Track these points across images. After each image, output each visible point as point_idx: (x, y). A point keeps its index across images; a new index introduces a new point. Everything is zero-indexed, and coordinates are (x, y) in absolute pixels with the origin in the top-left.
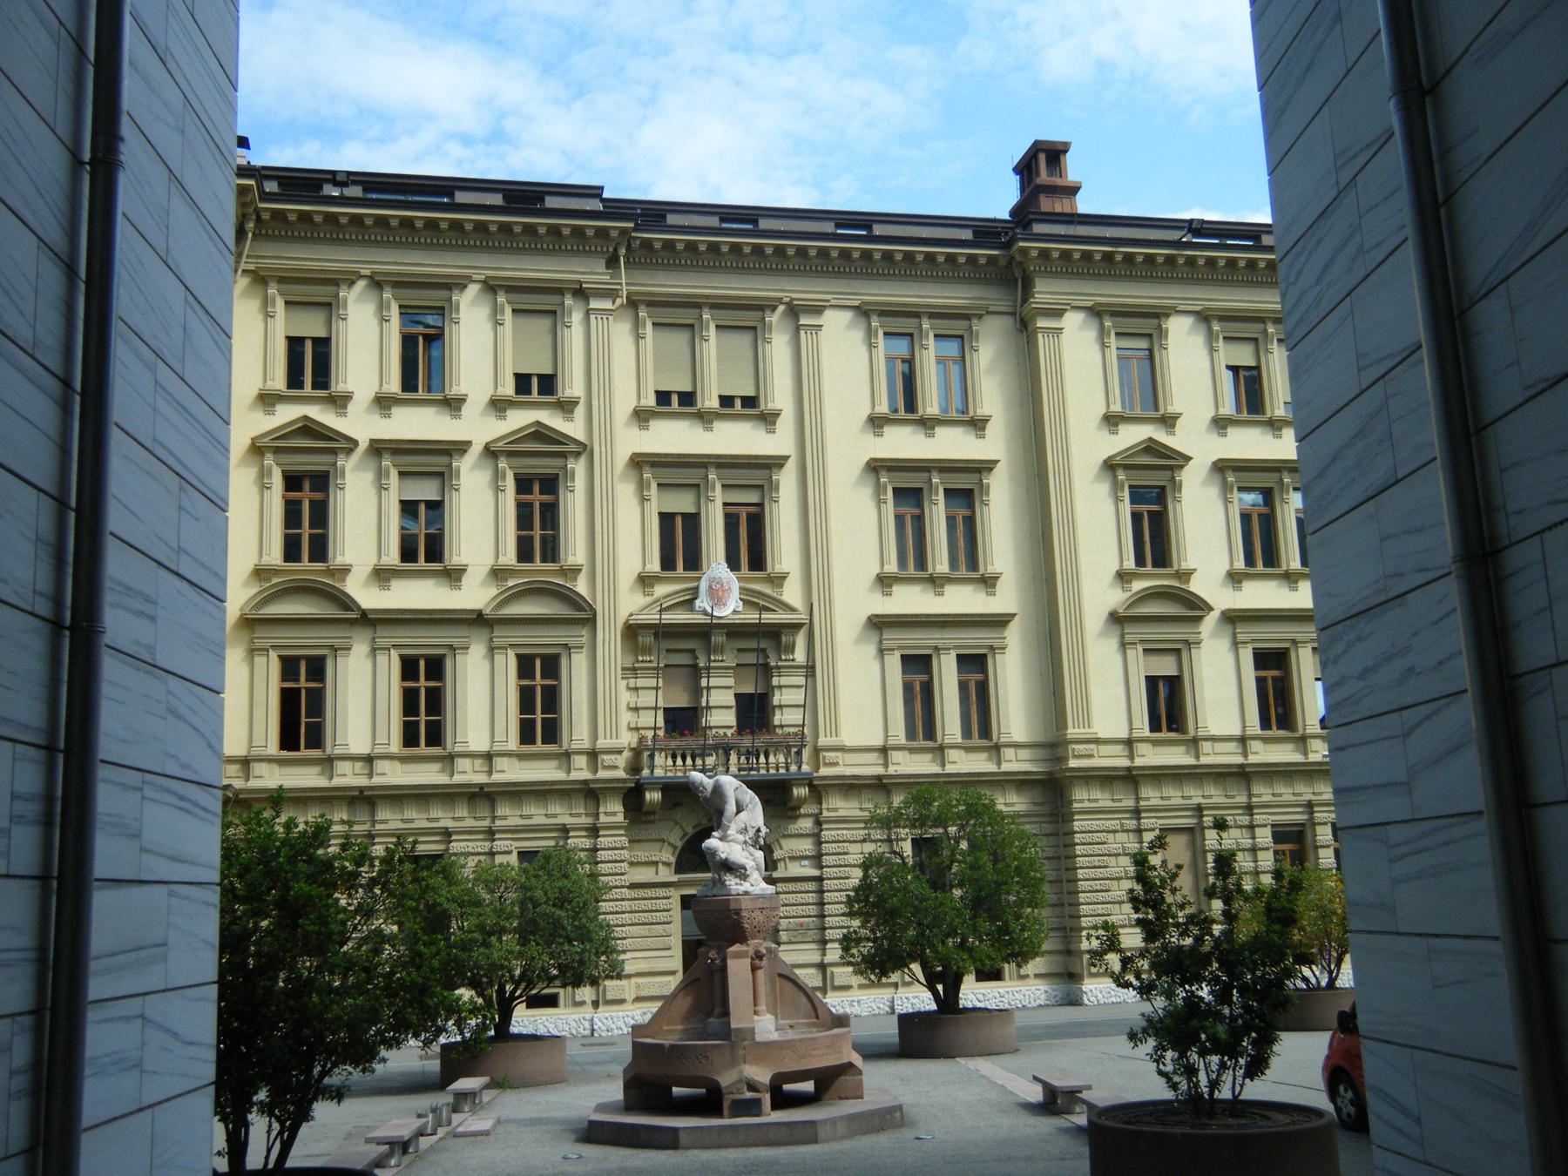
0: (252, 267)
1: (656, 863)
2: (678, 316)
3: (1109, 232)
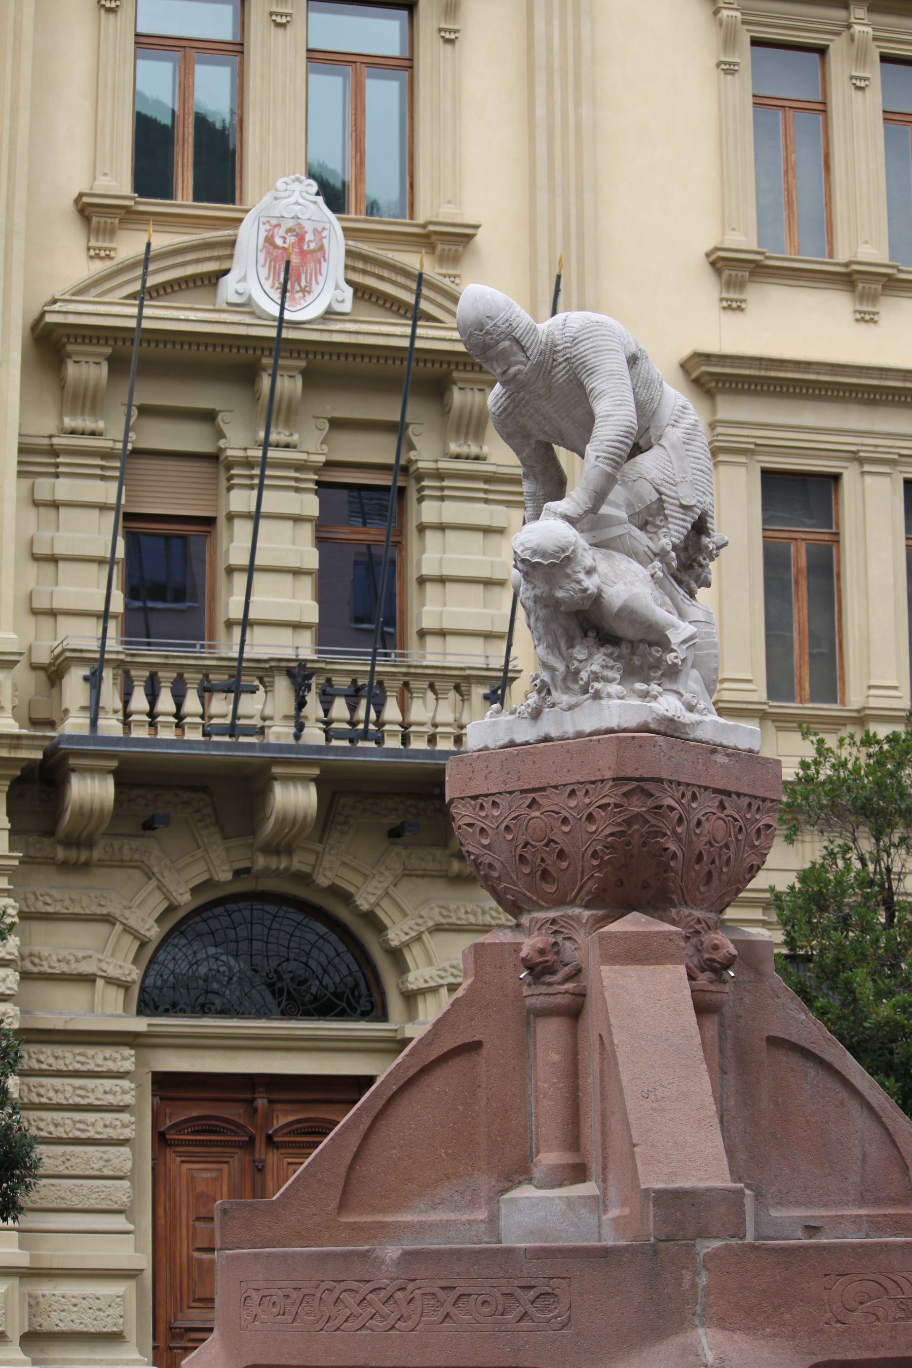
1: (89, 979)
3: (197, 1159)
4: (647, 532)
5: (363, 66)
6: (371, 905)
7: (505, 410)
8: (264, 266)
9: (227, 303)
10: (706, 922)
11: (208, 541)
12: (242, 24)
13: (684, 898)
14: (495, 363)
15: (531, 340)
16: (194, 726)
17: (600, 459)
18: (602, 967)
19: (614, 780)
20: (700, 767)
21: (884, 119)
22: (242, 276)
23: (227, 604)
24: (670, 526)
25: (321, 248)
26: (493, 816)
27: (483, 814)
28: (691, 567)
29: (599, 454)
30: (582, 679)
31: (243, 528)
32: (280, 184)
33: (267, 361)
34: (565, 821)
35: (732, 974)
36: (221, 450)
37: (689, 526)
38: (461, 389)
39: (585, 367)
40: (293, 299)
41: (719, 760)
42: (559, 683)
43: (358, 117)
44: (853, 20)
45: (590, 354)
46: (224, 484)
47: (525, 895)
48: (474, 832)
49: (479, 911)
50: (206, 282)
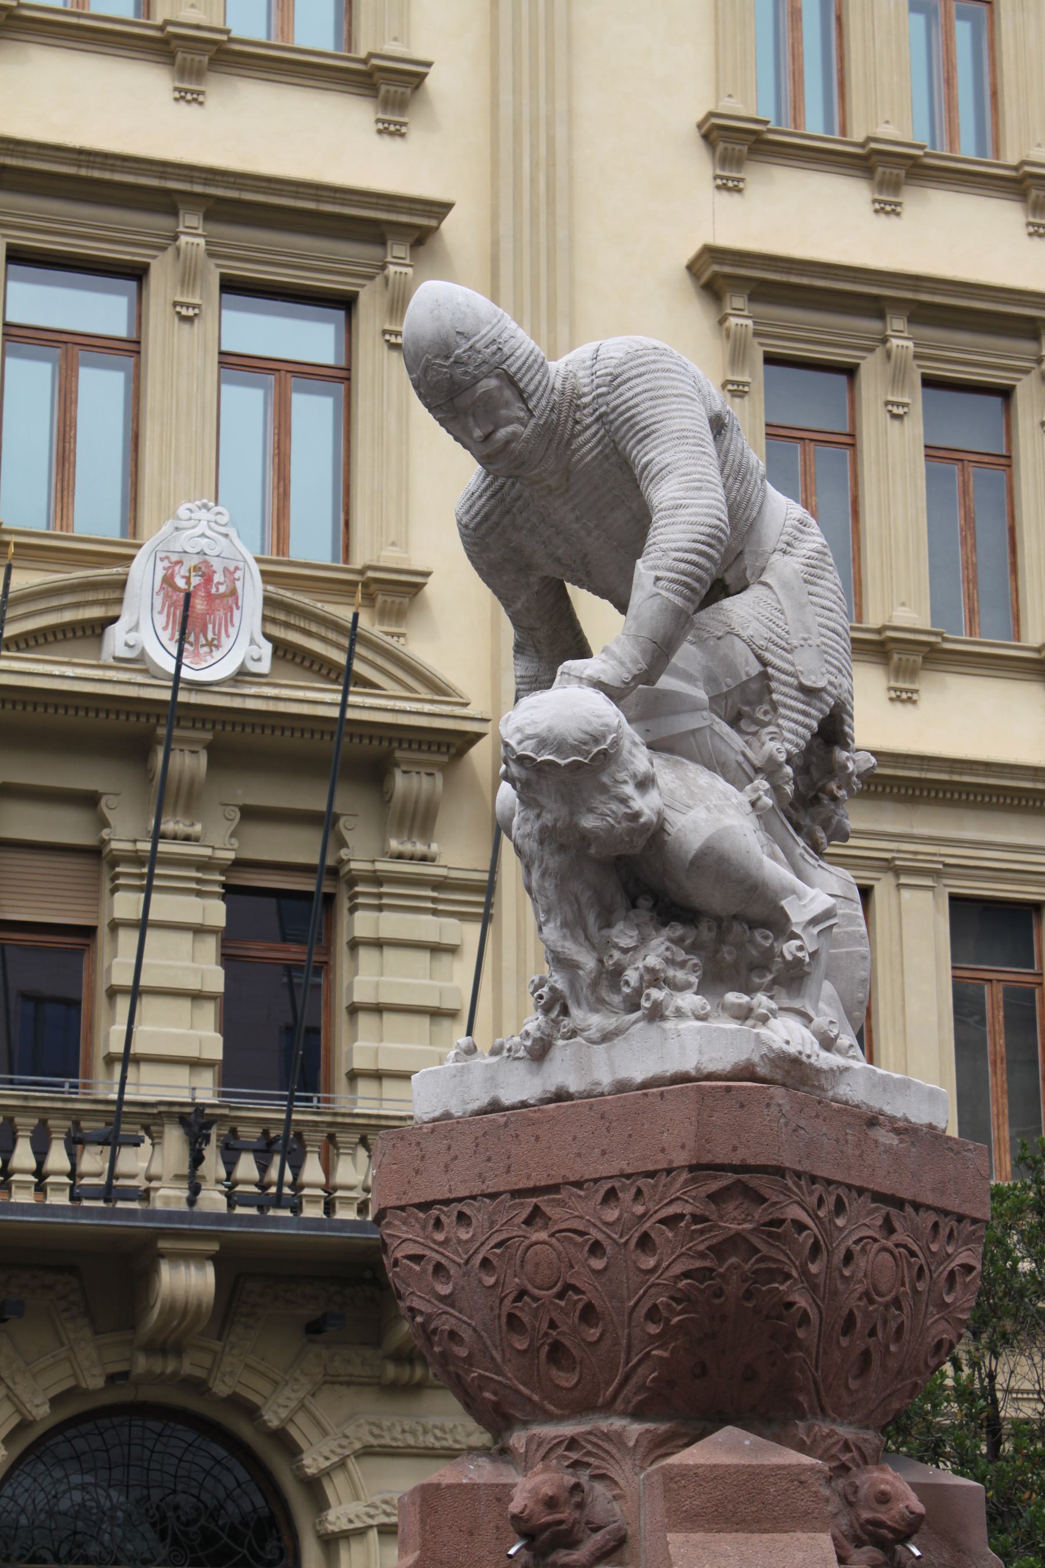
4: (740, 731)
5: (289, 375)
6: (282, 1420)
7: (486, 518)
8: (161, 612)
9: (114, 658)
10: (859, 1449)
11: (86, 955)
12: (138, 317)
13: (819, 1400)
14: (471, 419)
15: (535, 382)
16: (58, 1187)
17: (661, 583)
18: (670, 1537)
19: (691, 1168)
20: (849, 1150)
21: (926, 456)
22: (133, 624)
23: (108, 1035)
24: (781, 721)
25: (233, 593)
26: (459, 1241)
27: (440, 1237)
28: (816, 800)
29: (660, 574)
30: (627, 983)
31: (128, 940)
32: (182, 511)
33: (162, 731)
34: (596, 1249)
35: (917, 1553)
36: (104, 842)
37: (815, 724)
38: (405, 772)
39: (632, 427)
40: (196, 654)
41: (881, 1140)
42: (585, 991)
43: (282, 439)
44: (889, 332)
45: (643, 402)
46: (107, 885)
47: (518, 1392)
48: (424, 1271)
49: (420, 1429)
50: (89, 632)
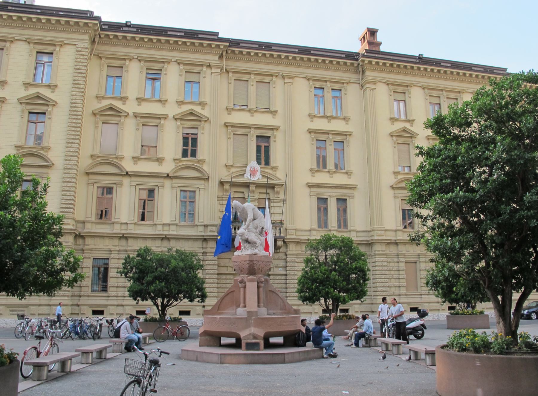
0: (96, 54)
1: (227, 267)
2: (242, 77)
